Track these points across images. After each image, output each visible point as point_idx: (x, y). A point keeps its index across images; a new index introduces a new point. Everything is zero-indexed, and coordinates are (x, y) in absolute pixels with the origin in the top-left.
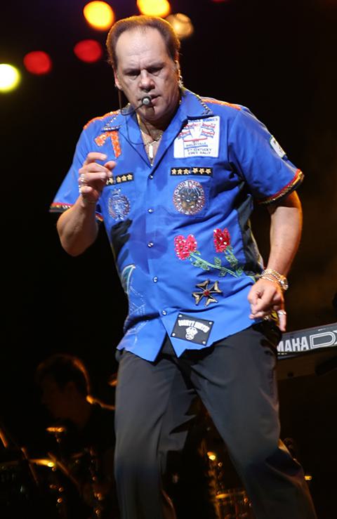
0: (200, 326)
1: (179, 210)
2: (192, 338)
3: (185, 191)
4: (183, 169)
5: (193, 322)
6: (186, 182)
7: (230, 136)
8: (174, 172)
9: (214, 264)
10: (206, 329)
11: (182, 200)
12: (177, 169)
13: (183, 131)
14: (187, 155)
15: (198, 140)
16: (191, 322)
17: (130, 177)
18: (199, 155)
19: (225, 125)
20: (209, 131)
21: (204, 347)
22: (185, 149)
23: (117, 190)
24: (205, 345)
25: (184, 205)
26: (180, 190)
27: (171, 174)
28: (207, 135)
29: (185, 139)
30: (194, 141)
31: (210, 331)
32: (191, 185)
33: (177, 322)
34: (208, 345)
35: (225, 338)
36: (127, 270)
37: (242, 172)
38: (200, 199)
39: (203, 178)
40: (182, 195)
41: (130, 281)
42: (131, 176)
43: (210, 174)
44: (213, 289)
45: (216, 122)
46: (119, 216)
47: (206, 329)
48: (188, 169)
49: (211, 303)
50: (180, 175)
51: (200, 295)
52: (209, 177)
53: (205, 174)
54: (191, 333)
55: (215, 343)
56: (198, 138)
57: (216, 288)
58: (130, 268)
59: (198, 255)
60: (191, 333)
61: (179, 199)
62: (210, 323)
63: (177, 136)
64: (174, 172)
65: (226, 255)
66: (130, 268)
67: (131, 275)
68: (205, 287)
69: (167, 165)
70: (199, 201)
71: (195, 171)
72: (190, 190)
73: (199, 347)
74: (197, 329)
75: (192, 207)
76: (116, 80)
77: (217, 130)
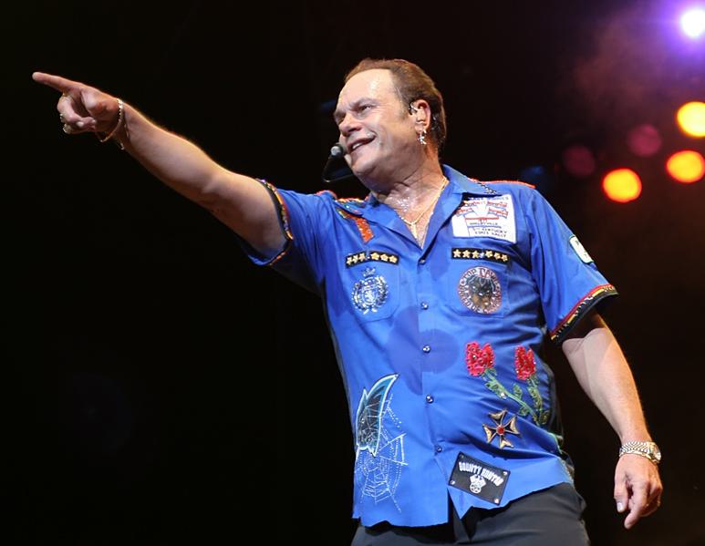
0: (489, 474)
1: (470, 307)
2: (479, 491)
3: (476, 281)
4: (471, 250)
5: (480, 468)
6: (477, 269)
7: (489, 192)
8: (457, 253)
9: (513, 394)
10: (498, 481)
11: (472, 293)
12: (462, 250)
13: (463, 208)
14: (473, 235)
15: (486, 219)
16: (476, 467)
17: (393, 259)
18: (490, 235)
19: (517, 202)
20: (499, 210)
21: (496, 507)
22: (469, 227)
23: (371, 269)
24: (498, 504)
25: (476, 299)
26: (468, 280)
27: (453, 257)
28: (498, 215)
29: (467, 216)
30: (481, 219)
31: (503, 485)
32: (484, 274)
33: (456, 465)
34: (503, 505)
35: (526, 496)
36: (386, 381)
37: (558, 248)
38: (494, 296)
39: (496, 266)
40: (471, 285)
41: (387, 398)
42: (348, 262)
43: (505, 263)
44: (508, 427)
45: (507, 200)
46: (370, 307)
47: (498, 481)
48: (479, 251)
49: (506, 446)
50: (466, 258)
51: (493, 431)
52: (505, 266)
53: (500, 260)
54: (477, 483)
55: (511, 503)
56: (485, 216)
57: (512, 426)
58: (390, 380)
59: (493, 375)
60: (477, 483)
61: (467, 292)
62: (506, 473)
63: (455, 212)
64: (457, 253)
65: (528, 386)
66: (390, 380)
67: (390, 389)
68: (498, 421)
69: (442, 251)
70: (493, 298)
71: (489, 254)
72: (483, 280)
73: (490, 506)
74: (486, 480)
75: (486, 304)
76: (588, 259)
77: (510, 209)
